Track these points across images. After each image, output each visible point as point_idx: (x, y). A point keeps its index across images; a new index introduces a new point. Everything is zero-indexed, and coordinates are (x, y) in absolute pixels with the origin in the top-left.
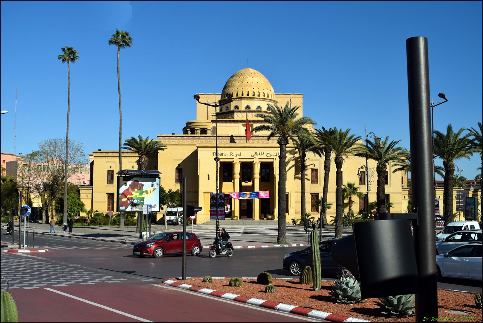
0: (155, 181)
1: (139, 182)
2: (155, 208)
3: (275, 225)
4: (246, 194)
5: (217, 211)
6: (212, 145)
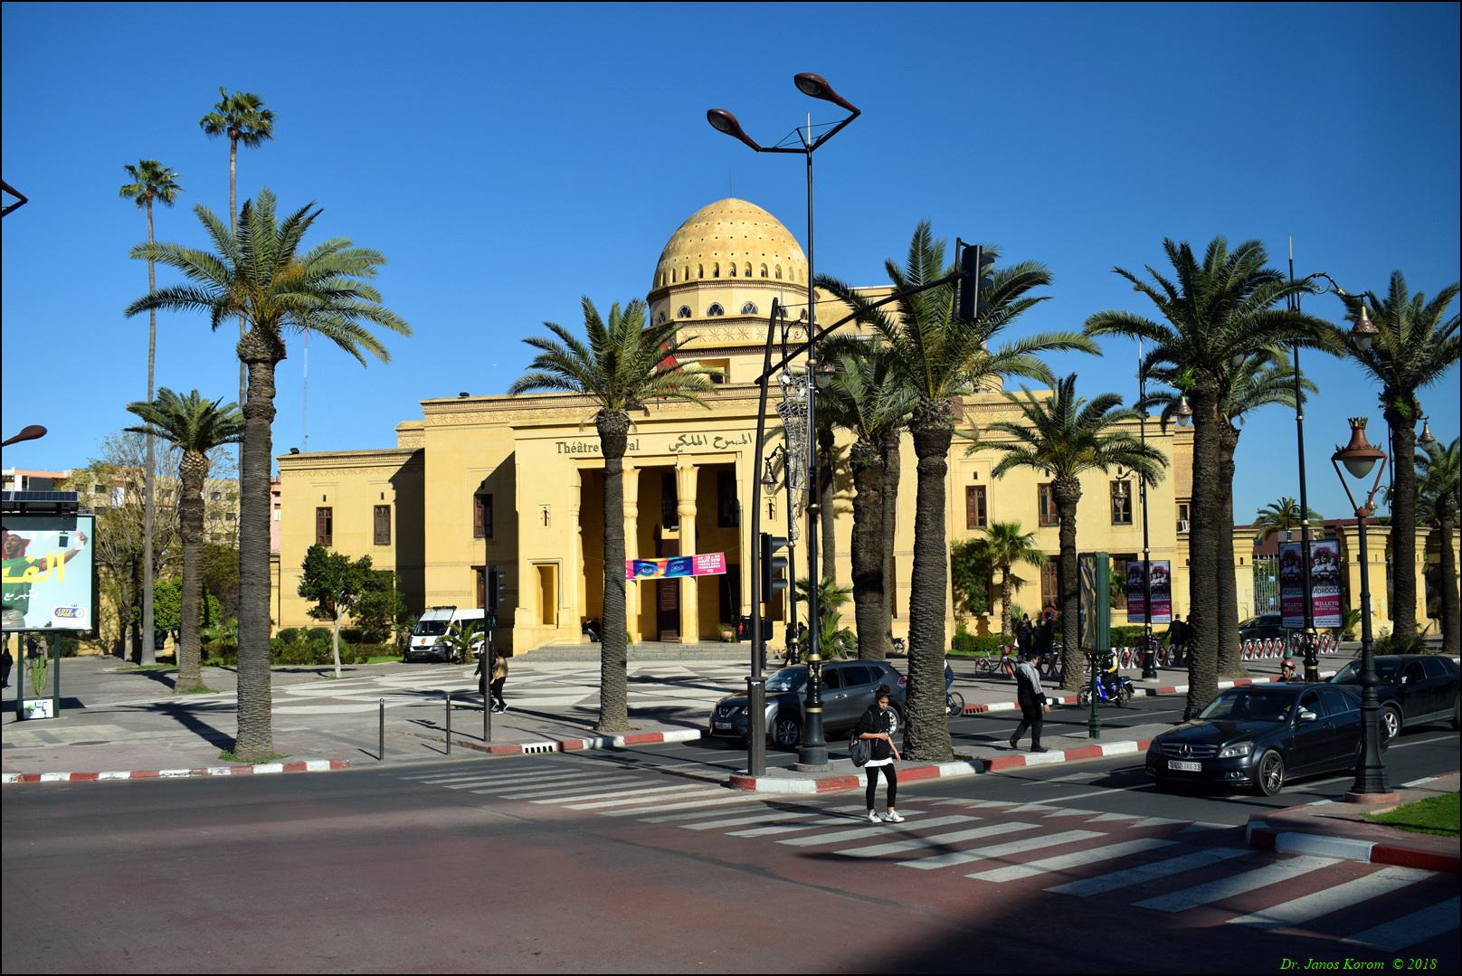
0: (74, 528)
1: (10, 533)
2: (74, 616)
3: (723, 659)
4: (655, 564)
6: (555, 419)
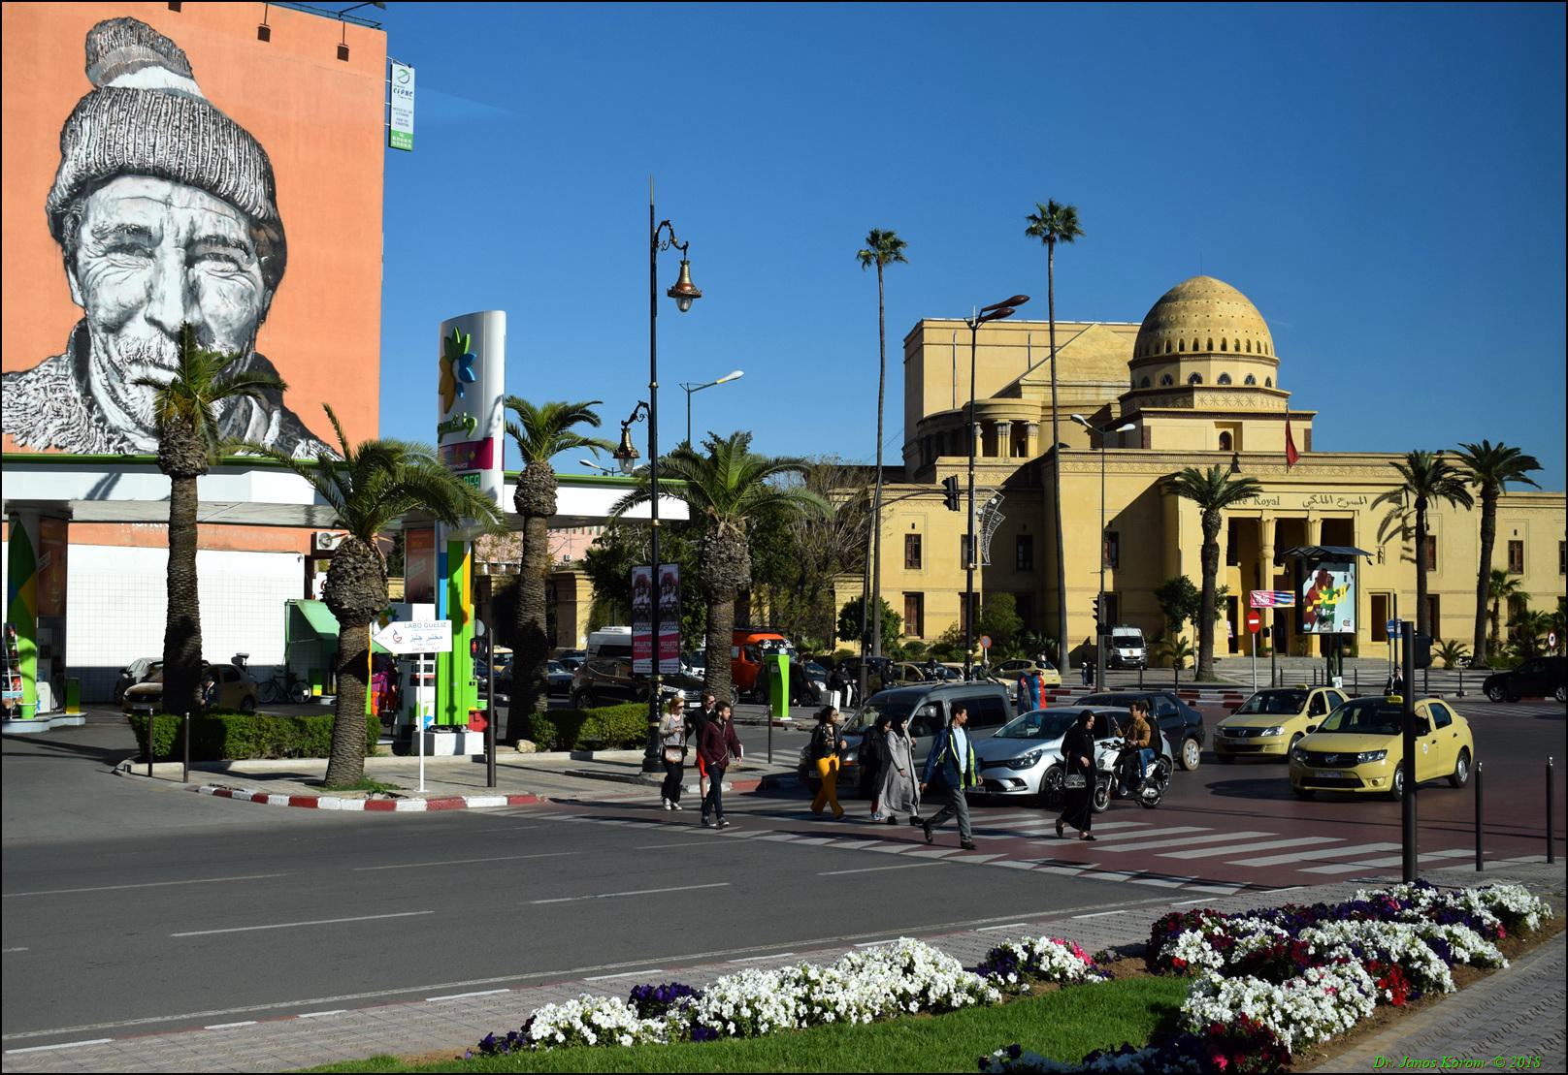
5: (655, 638)
